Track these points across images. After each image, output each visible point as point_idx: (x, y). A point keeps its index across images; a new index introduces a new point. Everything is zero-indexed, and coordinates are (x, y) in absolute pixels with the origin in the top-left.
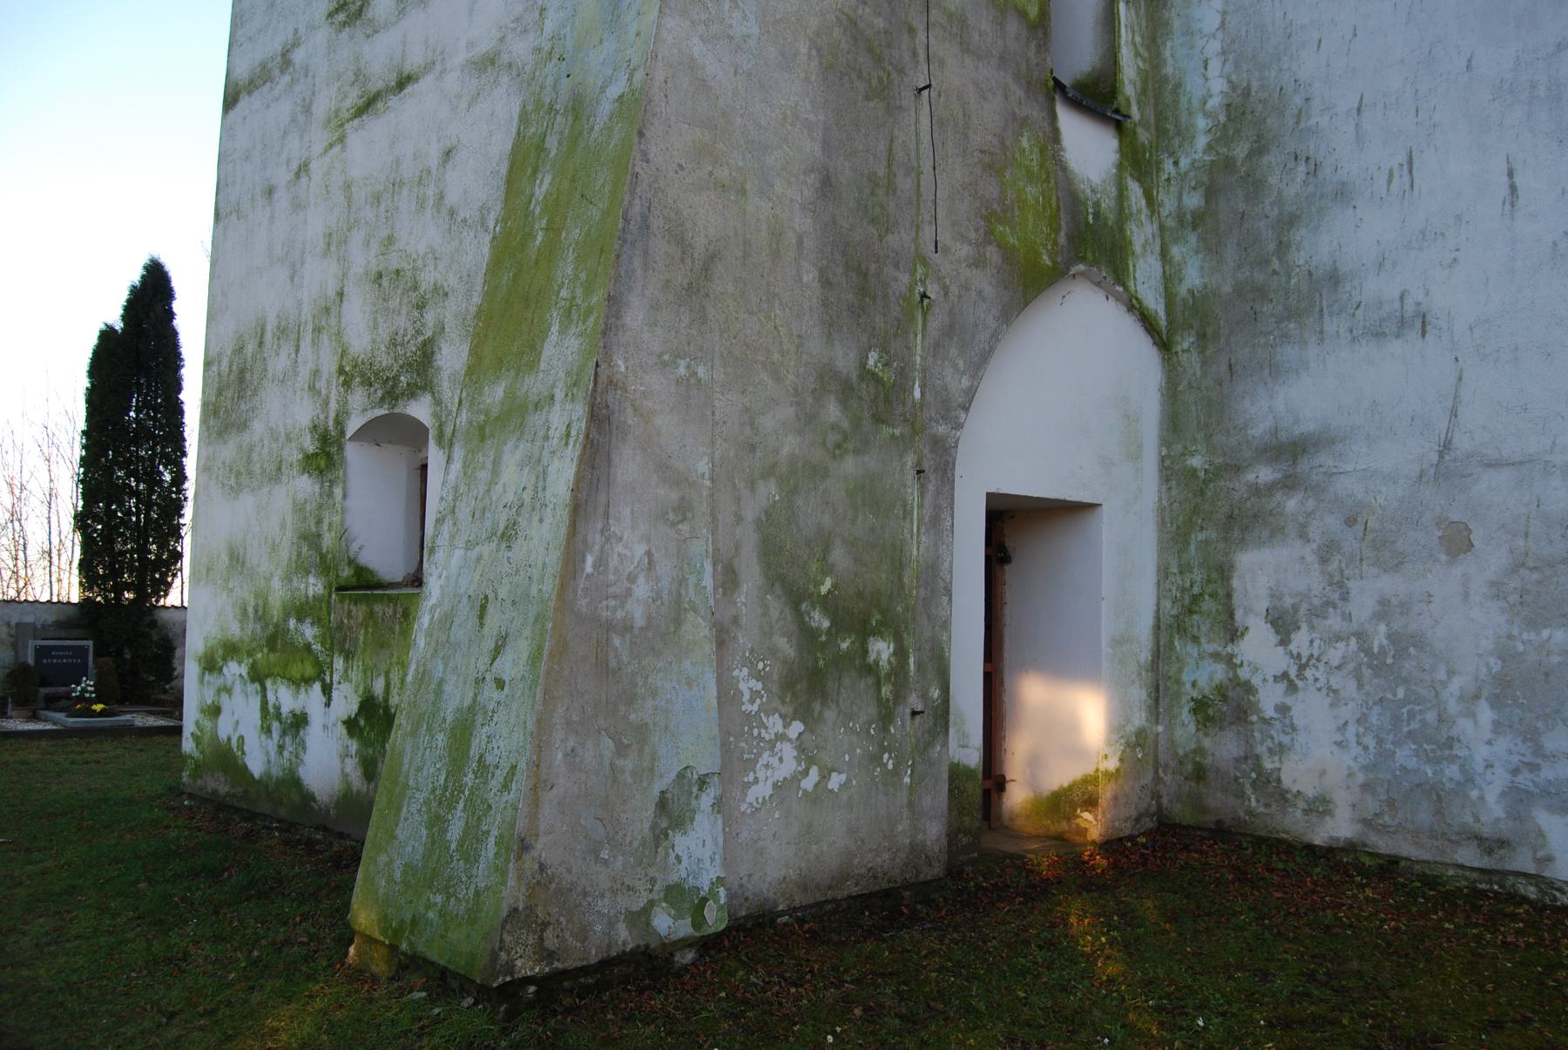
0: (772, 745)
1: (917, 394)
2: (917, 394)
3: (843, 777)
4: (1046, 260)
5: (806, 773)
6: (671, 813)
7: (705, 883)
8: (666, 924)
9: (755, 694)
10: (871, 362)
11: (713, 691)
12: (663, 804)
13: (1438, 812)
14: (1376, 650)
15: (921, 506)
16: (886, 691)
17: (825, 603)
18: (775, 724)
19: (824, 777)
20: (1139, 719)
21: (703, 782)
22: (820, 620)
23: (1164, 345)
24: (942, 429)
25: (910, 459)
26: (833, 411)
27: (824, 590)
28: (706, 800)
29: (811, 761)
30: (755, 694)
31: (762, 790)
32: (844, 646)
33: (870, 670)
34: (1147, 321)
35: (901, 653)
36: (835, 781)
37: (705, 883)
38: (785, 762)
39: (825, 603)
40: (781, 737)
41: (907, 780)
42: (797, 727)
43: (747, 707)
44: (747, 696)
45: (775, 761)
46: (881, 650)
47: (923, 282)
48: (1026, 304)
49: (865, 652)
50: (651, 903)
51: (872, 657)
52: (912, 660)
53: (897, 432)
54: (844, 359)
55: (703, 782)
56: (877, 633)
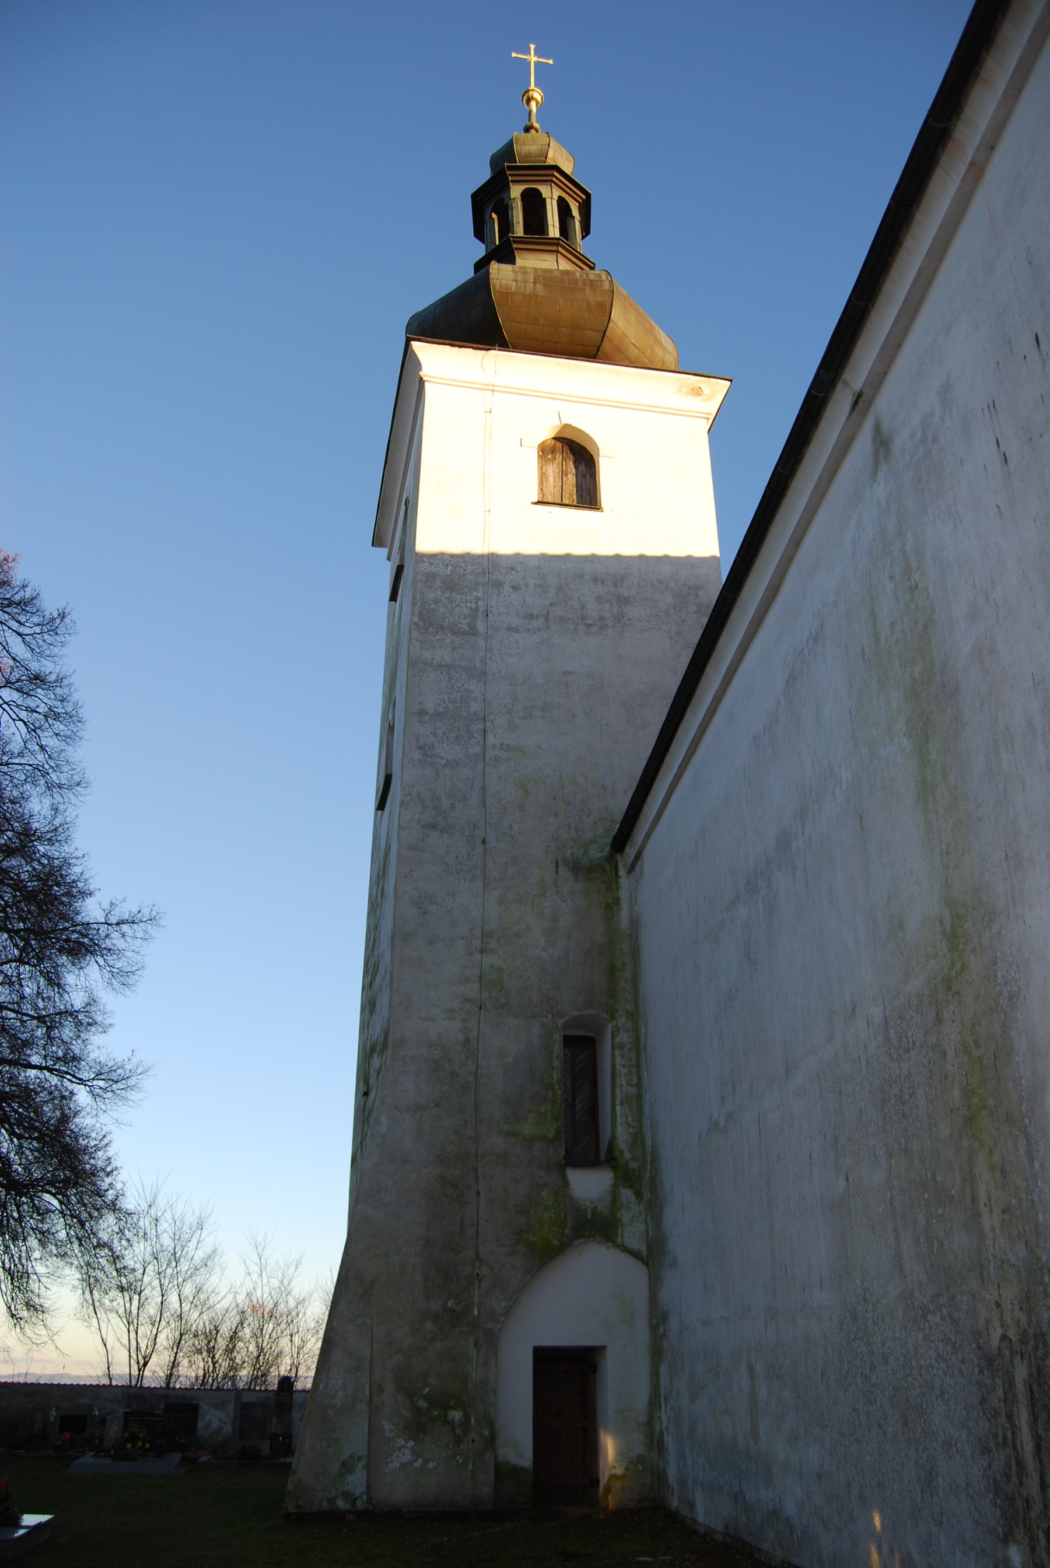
0: (400, 1449)
1: (476, 1312)
2: (476, 1312)
3: (435, 1464)
4: (556, 1242)
5: (416, 1460)
6: (347, 1468)
7: (358, 1493)
8: (341, 1504)
9: (391, 1431)
10: (449, 1305)
11: (367, 1429)
12: (343, 1464)
13: (463, 939)
14: (467, 629)
15: (477, 1357)
16: (458, 1431)
17: (425, 1397)
18: (401, 1441)
19: (426, 1462)
20: (639, 1449)
21: (359, 1458)
22: (423, 1404)
23: (647, 1264)
24: (490, 1325)
25: (471, 1339)
26: (429, 1325)
27: (425, 1392)
28: (361, 1465)
29: (418, 1456)
30: (391, 1431)
31: (395, 1465)
32: (435, 1413)
33: (451, 1423)
34: (635, 1255)
35: (466, 1416)
36: (430, 1465)
37: (358, 1493)
38: (407, 1456)
39: (425, 1397)
40: (405, 1447)
41: (470, 1467)
42: (411, 1443)
43: (388, 1435)
44: (388, 1431)
45: (401, 1455)
46: (456, 1415)
47: (479, 1268)
48: (542, 1266)
49: (446, 1416)
50: (336, 1497)
51: (450, 1418)
52: (472, 1419)
53: (464, 1330)
54: (435, 1305)
55: (359, 1458)
56: (453, 1408)
